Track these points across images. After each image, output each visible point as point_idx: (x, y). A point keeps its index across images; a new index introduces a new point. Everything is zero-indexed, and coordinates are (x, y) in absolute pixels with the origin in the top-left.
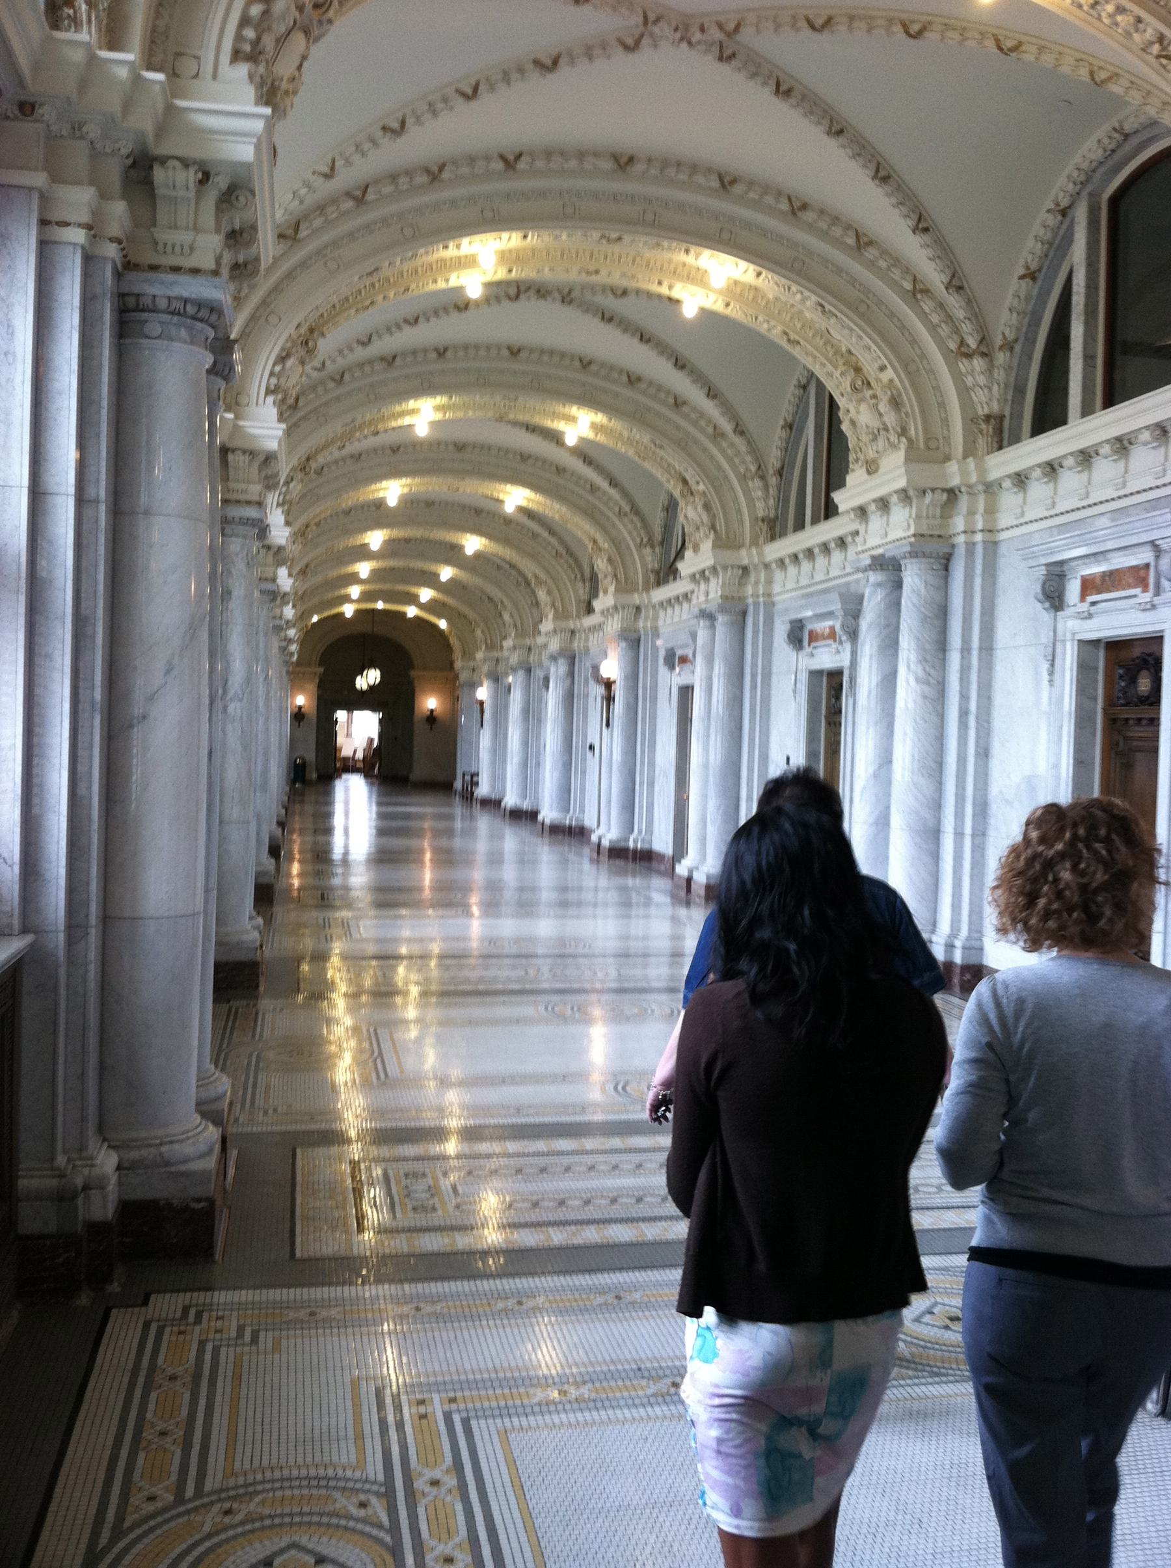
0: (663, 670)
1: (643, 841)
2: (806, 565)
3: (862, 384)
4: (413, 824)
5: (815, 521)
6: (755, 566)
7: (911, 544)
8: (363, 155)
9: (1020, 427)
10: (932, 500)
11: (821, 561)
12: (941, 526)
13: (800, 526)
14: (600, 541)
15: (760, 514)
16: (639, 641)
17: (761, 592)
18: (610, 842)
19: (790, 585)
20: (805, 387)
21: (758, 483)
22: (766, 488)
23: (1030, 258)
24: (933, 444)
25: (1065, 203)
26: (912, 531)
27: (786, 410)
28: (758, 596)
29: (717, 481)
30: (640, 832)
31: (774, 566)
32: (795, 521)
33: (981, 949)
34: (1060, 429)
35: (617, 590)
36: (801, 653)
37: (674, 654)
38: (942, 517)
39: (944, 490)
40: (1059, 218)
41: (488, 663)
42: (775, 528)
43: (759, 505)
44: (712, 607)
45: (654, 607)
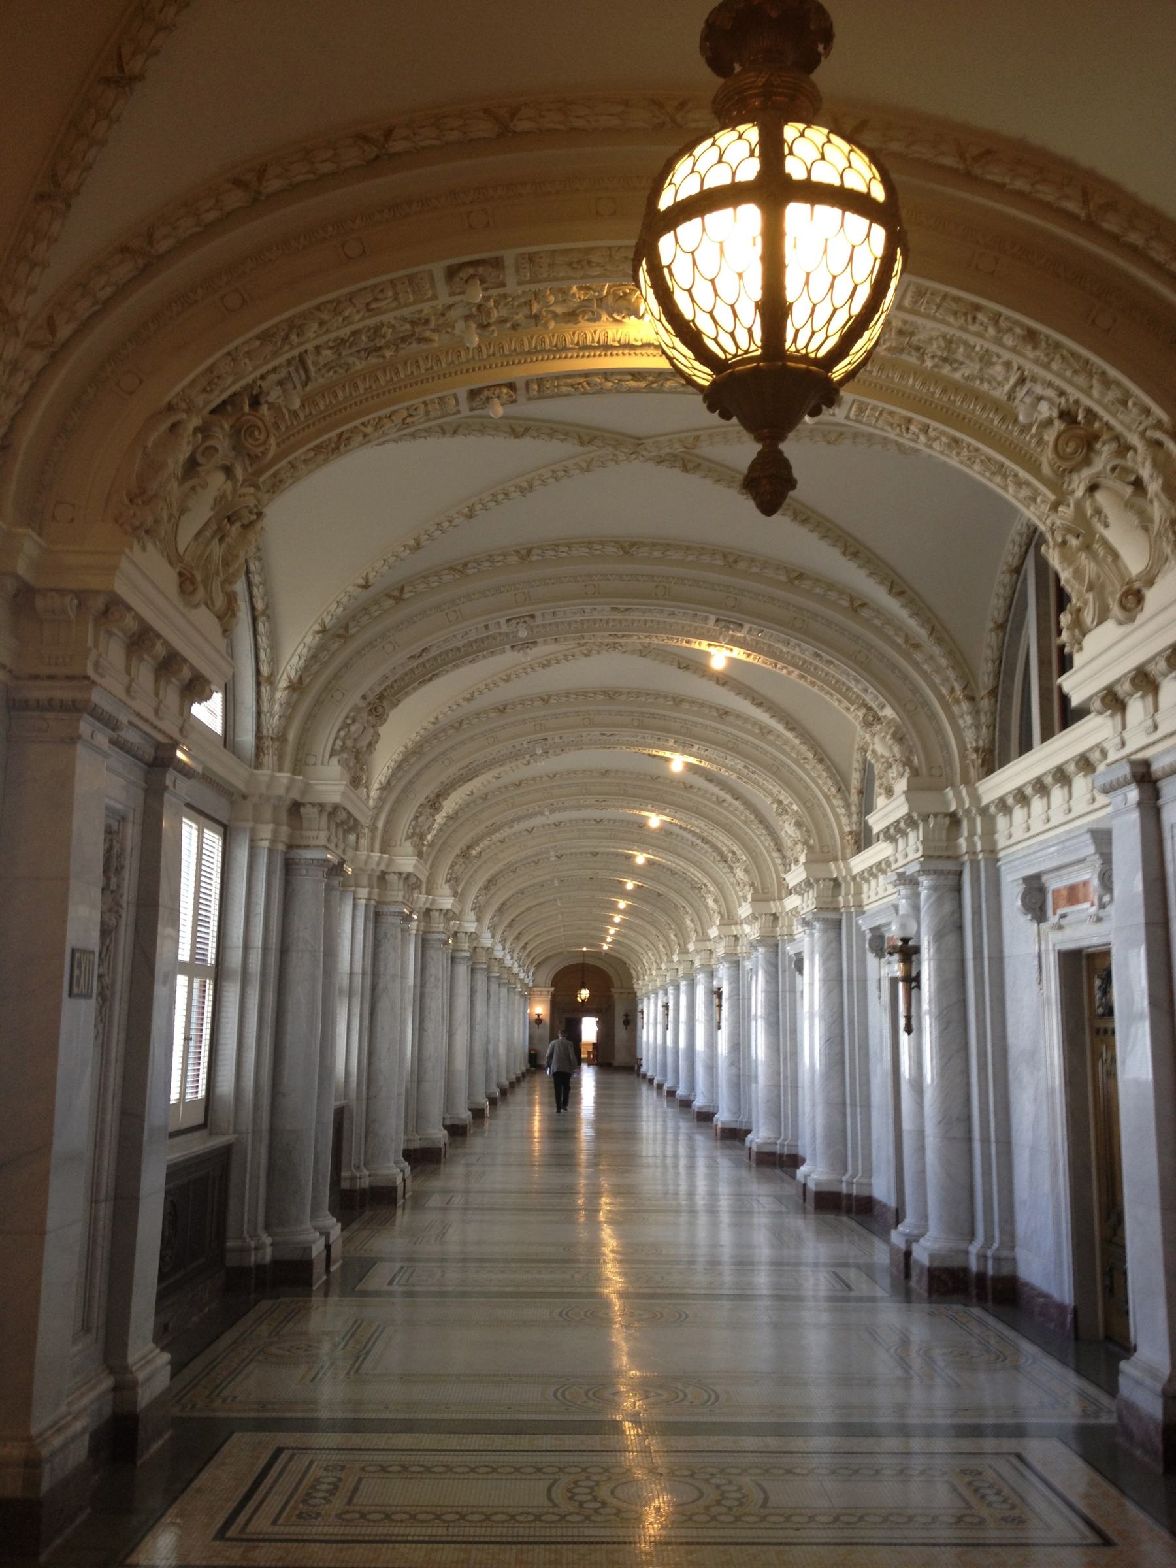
0: (871, 958)
1: (997, 1260)
2: (1058, 794)
3: (784, 810)
4: (201, 593)
5: (1047, 735)
6: (967, 812)
7: (921, 863)
8: (556, 479)
9: (1008, 748)
10: (935, 824)
11: (1037, 804)
12: (947, 848)
13: (1026, 746)
14: (738, 852)
15: (847, 829)
16: (840, 921)
17: (979, 848)
18: (932, 1257)
19: (1057, 817)
20: (1018, 570)
21: (965, 706)
22: (976, 713)
23: (996, 614)
24: (825, 849)
25: (1015, 564)
26: (920, 853)
27: (995, 607)
28: (975, 853)
29: (809, 804)
30: (989, 1239)
31: (993, 809)
32: (1020, 744)
33: (870, 1185)
34: (1080, 723)
35: (754, 900)
36: (1043, 926)
37: (1042, 890)
38: (948, 839)
39: (946, 815)
40: (1015, 576)
41: (723, 944)
42: (992, 760)
43: (844, 820)
44: (809, 917)
45: (854, 878)
